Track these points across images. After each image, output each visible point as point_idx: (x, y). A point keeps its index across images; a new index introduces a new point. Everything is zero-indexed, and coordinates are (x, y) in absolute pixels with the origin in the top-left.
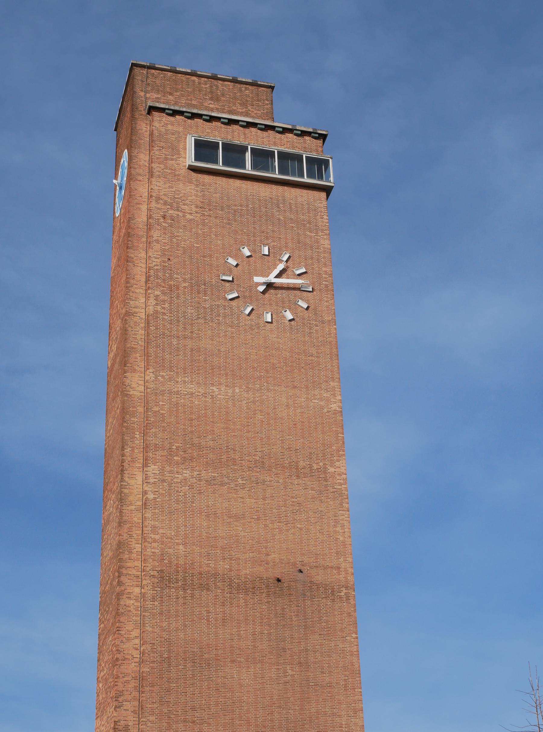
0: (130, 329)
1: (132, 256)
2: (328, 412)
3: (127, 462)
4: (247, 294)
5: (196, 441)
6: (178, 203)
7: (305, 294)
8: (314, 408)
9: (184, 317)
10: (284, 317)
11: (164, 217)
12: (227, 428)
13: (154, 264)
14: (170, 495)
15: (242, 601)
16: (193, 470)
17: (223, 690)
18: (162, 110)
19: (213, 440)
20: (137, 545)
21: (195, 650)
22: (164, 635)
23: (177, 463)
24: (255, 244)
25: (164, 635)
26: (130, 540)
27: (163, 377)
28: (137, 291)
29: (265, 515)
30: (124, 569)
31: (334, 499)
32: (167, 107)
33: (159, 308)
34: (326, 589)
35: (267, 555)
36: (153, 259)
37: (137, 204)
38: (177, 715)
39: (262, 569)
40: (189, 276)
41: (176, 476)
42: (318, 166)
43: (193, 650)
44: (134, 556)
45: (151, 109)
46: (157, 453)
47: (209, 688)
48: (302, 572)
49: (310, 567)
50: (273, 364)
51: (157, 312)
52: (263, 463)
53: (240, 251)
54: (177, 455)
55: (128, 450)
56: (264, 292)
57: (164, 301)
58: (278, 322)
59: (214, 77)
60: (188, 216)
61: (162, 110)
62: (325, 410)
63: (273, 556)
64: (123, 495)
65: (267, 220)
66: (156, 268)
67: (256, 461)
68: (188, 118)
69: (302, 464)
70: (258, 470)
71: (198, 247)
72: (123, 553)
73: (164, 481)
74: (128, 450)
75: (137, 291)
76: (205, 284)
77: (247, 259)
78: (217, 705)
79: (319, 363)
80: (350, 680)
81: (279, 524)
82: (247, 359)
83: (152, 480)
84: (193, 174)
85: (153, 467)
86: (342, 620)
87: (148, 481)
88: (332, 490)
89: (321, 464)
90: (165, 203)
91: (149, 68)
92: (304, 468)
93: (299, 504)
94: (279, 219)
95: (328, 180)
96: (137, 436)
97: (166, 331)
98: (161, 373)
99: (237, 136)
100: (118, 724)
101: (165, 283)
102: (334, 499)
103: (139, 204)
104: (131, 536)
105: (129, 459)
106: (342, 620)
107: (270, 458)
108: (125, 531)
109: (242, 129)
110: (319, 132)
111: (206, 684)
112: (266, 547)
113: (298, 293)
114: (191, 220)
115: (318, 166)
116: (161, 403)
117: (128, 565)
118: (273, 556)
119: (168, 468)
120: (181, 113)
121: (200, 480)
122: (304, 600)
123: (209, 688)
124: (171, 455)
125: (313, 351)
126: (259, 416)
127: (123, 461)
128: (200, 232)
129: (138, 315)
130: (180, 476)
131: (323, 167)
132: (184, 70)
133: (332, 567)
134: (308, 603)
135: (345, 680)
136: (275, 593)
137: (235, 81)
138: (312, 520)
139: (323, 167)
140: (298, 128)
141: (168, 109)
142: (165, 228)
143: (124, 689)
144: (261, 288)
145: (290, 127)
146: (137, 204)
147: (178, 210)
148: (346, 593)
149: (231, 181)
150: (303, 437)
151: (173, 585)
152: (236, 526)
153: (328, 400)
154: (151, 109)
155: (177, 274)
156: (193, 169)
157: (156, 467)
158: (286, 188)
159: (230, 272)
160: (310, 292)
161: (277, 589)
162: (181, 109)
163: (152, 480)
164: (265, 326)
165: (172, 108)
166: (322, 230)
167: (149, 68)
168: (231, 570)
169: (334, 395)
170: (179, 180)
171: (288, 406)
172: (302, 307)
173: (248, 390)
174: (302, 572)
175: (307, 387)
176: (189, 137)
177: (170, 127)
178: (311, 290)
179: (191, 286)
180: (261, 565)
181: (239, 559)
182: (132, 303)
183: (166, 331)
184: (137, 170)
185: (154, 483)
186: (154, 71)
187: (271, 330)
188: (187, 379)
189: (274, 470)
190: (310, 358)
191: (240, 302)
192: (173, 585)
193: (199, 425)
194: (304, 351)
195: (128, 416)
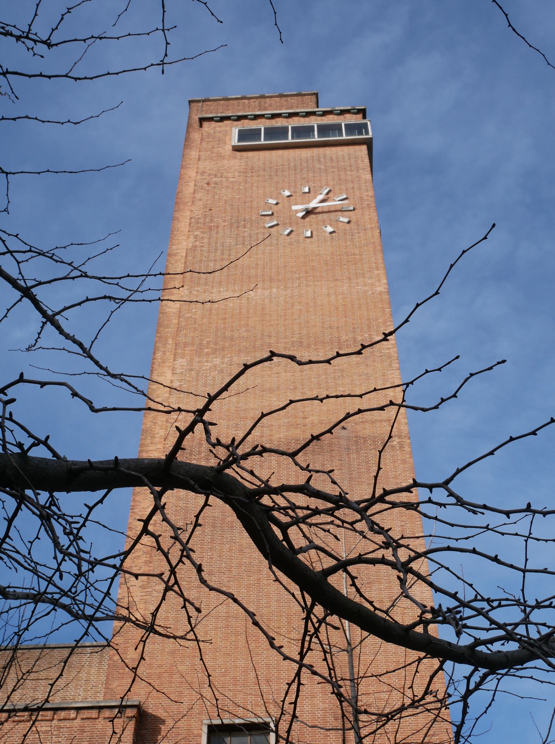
0: (170, 265)
1: (178, 216)
2: (372, 294)
3: (157, 363)
4: (287, 221)
5: (228, 334)
6: (222, 173)
7: (347, 213)
8: (357, 293)
9: (223, 246)
10: (325, 231)
11: (208, 184)
12: (262, 320)
13: (195, 214)
14: (197, 380)
15: (274, 463)
16: (224, 357)
17: (248, 550)
18: (211, 119)
19: (247, 331)
20: (161, 430)
21: (216, 514)
22: (181, 504)
23: (208, 354)
24: (296, 188)
25: (181, 504)
26: (154, 427)
27: (197, 291)
28: (181, 238)
29: (303, 385)
30: (144, 453)
31: (382, 361)
32: (215, 115)
33: (198, 243)
34: (374, 441)
35: (305, 418)
36: (195, 212)
37: (185, 182)
38: (190, 582)
39: (298, 431)
40: (229, 217)
41: (205, 364)
42: (361, 128)
43: (214, 515)
44: (157, 440)
45: (202, 120)
46: (186, 349)
47: (231, 550)
48: (345, 429)
49: (355, 423)
50: (313, 266)
51: (195, 246)
52: (301, 342)
53: (280, 193)
54: (207, 348)
55: (159, 354)
56: (303, 217)
57: (203, 238)
58: (318, 236)
59: (263, 97)
60: (231, 180)
61: (211, 119)
62: (370, 293)
63: (311, 418)
64: (150, 390)
65: (308, 171)
66: (197, 217)
67: (293, 343)
68: (235, 120)
69: (344, 338)
70: (296, 348)
71: (239, 198)
72: (145, 439)
73: (191, 370)
74: (159, 355)
75: (181, 238)
76: (244, 221)
77: (288, 198)
78: (240, 565)
79: (361, 259)
80: (408, 525)
81: (319, 390)
82: (285, 266)
83: (178, 371)
84: (237, 153)
85: (181, 360)
86: (395, 467)
87: (175, 372)
88: (379, 355)
89: (366, 335)
90: (210, 175)
91: (204, 101)
92: (347, 340)
93: (342, 371)
94: (320, 169)
95: (367, 133)
96: (170, 342)
97: (204, 258)
98: (196, 289)
99: (279, 123)
100: (122, 601)
101: (205, 226)
102: (382, 361)
103: (188, 182)
104: (155, 424)
105: (160, 361)
106: (395, 467)
107: (309, 337)
108: (150, 419)
109: (285, 119)
110: (357, 108)
111: (228, 546)
112: (303, 412)
113: (340, 213)
114: (234, 182)
115: (361, 128)
116: (194, 310)
117: (150, 448)
118: (311, 418)
119: (197, 359)
120: (228, 118)
121: (231, 365)
122: (348, 454)
123: (231, 550)
124: (201, 349)
125: (356, 251)
126: (297, 307)
127: (153, 364)
128: (242, 187)
129: (180, 254)
130: (209, 364)
131: (364, 130)
132: (235, 97)
133: (381, 421)
134: (354, 456)
135: (402, 526)
136: (314, 451)
137: (281, 96)
138: (357, 382)
139: (364, 130)
140: (336, 108)
141: (216, 117)
142: (208, 190)
143: (132, 565)
144: (301, 214)
145: (329, 109)
146: (185, 182)
147: (222, 177)
148: (399, 443)
149: (274, 152)
150: (346, 317)
151: (195, 457)
152: (270, 397)
153: (372, 285)
154: (202, 120)
155: (218, 218)
156: (236, 149)
157: (185, 360)
158: (327, 148)
159: (271, 208)
160: (351, 211)
161: (316, 447)
162: (228, 115)
163: (178, 371)
164: (304, 241)
165: (219, 115)
166: (363, 169)
167: (204, 101)
168: (262, 436)
169: (379, 280)
170: (224, 159)
171: (329, 295)
172: (343, 222)
173: (286, 288)
174: (345, 429)
175: (349, 279)
176: (234, 129)
177: (218, 129)
178: (352, 209)
179: (231, 224)
180: (297, 428)
181: (272, 425)
182: (174, 247)
183: (204, 258)
184: (188, 162)
185: (181, 373)
186: (208, 103)
187: (311, 243)
188: (222, 289)
189: (313, 346)
190: (352, 257)
191: (279, 228)
192: (195, 457)
193: (232, 322)
194: (346, 253)
195: (162, 328)
